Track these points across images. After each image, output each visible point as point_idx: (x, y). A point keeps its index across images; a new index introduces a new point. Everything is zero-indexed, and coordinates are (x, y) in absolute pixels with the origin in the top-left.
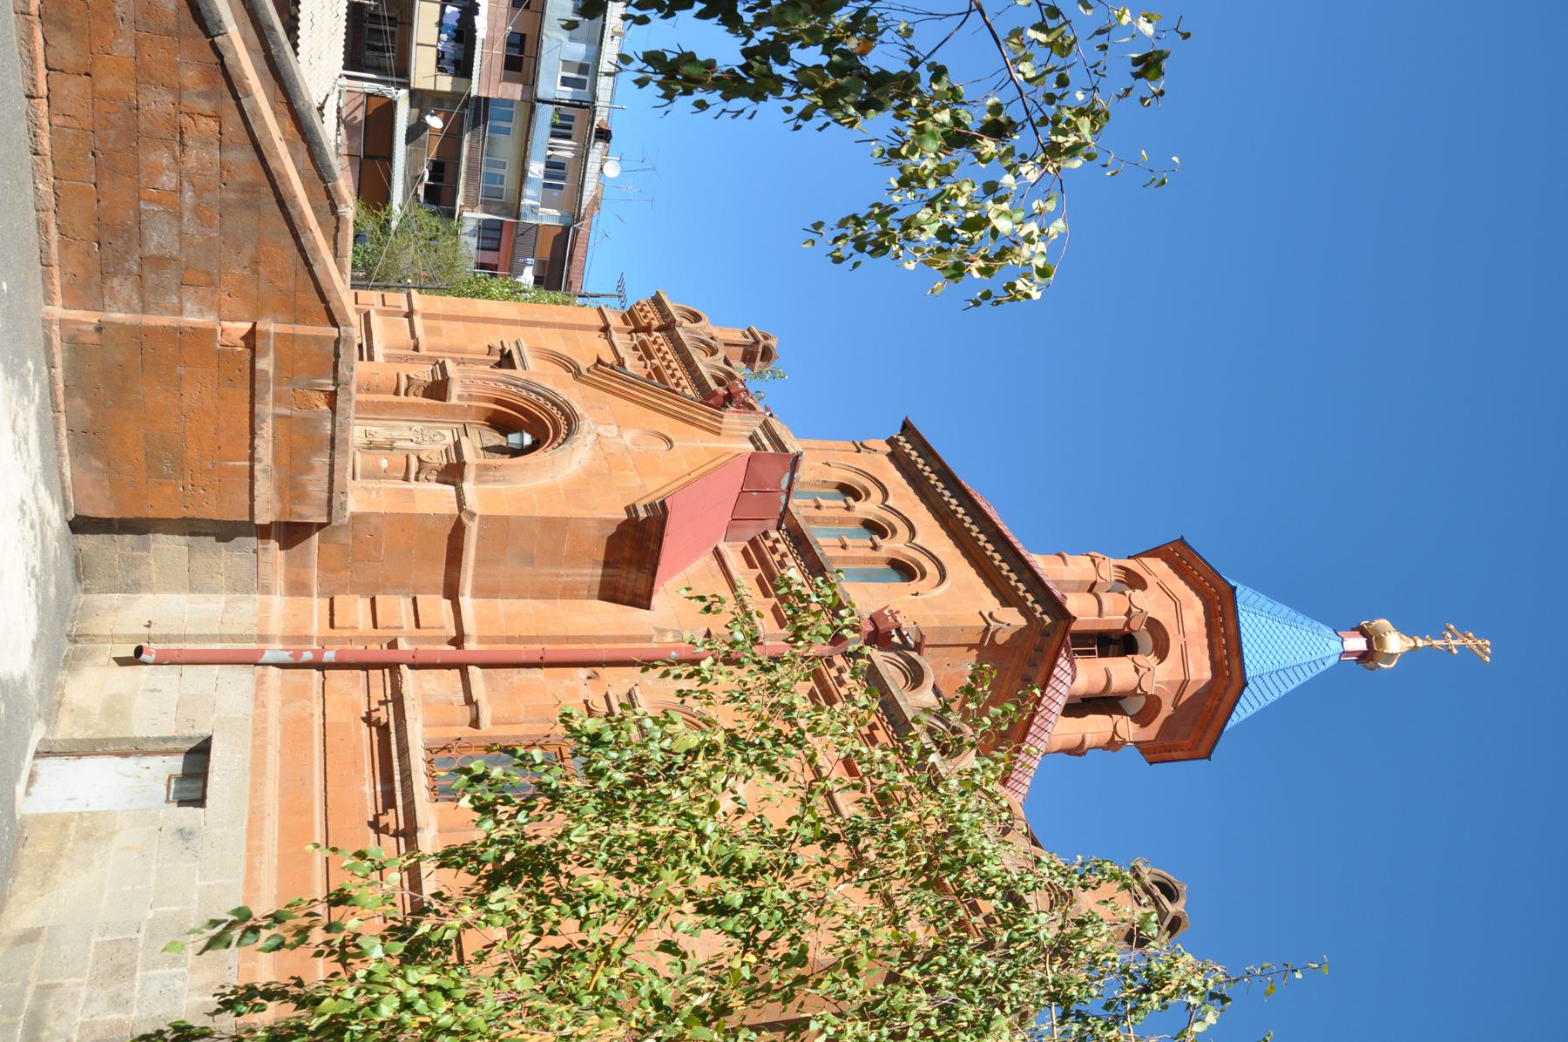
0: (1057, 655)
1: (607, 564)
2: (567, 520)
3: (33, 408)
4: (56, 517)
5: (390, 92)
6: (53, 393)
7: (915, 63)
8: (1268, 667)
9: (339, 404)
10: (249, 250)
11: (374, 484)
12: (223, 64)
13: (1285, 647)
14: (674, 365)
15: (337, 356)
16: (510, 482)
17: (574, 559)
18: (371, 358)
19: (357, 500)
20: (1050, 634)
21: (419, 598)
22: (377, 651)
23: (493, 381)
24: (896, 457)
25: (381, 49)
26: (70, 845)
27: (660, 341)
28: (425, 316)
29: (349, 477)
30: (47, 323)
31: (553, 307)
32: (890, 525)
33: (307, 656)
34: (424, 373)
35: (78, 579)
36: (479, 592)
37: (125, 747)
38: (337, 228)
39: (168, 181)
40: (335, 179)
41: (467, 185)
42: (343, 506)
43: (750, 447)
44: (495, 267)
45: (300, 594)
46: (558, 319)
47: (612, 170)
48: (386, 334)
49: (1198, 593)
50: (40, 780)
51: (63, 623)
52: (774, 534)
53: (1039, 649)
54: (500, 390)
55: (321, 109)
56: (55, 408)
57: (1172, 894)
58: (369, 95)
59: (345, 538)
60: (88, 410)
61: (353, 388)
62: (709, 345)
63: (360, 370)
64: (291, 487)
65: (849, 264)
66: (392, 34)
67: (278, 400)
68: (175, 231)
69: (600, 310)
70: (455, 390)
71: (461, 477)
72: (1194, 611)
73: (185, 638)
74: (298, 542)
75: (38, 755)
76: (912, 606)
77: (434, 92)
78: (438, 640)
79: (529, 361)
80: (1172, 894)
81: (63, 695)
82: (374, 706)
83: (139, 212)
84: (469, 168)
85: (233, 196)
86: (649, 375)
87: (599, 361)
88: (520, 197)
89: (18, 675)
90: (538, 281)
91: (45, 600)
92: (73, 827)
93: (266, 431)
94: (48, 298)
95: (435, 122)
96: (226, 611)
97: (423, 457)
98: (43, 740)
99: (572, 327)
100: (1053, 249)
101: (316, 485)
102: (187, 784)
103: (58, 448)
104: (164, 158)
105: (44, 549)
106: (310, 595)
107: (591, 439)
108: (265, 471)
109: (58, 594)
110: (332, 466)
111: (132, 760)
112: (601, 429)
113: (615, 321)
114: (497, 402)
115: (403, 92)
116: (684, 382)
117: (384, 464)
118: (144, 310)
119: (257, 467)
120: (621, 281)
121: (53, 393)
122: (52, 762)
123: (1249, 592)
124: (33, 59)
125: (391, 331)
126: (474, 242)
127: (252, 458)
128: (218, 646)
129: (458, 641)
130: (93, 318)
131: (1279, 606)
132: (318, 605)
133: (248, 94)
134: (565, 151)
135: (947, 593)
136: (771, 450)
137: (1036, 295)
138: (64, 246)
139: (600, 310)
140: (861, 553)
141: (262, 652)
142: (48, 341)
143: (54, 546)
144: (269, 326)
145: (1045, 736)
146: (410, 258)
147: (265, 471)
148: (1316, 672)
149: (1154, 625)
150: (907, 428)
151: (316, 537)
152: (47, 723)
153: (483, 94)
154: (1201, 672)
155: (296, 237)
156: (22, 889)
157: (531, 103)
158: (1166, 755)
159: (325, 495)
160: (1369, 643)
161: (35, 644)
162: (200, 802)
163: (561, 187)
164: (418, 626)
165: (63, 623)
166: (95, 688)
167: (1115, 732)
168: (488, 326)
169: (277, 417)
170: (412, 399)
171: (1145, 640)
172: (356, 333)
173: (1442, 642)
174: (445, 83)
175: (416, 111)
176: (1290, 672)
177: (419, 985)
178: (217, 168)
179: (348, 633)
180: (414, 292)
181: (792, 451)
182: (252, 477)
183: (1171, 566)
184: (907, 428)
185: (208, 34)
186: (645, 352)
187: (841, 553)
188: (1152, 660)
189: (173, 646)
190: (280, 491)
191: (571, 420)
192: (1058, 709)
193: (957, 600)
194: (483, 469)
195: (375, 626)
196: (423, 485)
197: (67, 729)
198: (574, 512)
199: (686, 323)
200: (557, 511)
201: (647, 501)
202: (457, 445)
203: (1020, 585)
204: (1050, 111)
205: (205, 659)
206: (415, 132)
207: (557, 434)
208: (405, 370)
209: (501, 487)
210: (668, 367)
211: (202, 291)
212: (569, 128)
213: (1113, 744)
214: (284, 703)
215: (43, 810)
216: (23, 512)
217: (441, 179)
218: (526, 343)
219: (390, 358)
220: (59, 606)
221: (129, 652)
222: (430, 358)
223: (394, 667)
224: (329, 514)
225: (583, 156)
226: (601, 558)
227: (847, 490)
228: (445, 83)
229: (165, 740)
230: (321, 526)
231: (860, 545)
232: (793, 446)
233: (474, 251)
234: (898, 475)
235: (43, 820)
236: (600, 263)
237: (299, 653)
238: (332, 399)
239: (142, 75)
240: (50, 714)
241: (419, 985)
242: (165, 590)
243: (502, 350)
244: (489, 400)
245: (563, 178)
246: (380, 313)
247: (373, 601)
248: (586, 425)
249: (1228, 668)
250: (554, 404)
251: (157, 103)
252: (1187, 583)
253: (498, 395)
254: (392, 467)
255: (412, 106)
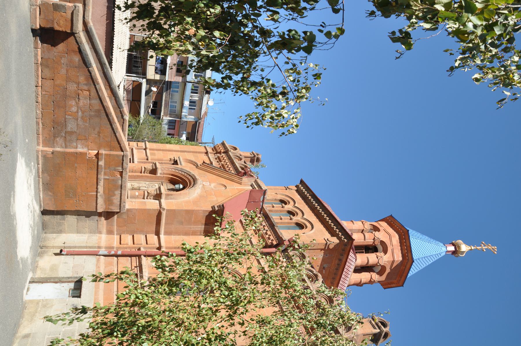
0: (349, 251)
1: (206, 224)
2: (193, 211)
3: (33, 176)
4: (38, 210)
5: (141, 80)
6: (38, 172)
7: (263, 78)
8: (421, 256)
9: (124, 175)
10: (97, 129)
11: (134, 200)
12: (91, 76)
13: (426, 250)
14: (228, 164)
15: (123, 160)
16: (176, 199)
17: (196, 223)
18: (133, 162)
19: (128, 205)
20: (347, 245)
21: (148, 235)
22: (134, 251)
23: (171, 169)
24: (298, 191)
25: (137, 67)
26: (39, 309)
27: (224, 156)
28: (150, 149)
29: (126, 197)
30: (38, 151)
31: (191, 146)
32: (296, 212)
33: (113, 253)
34: (149, 167)
35: (43, 229)
36: (166, 233)
37: (56, 280)
38: (123, 123)
39: (74, 109)
40: (123, 108)
41: (164, 109)
42: (124, 206)
43: (251, 188)
44: (173, 135)
45: (111, 234)
46: (192, 150)
47: (211, 103)
48: (138, 155)
49: (397, 232)
50: (31, 290)
51: (38, 242)
52: (259, 215)
53: (343, 250)
54: (173, 171)
55: (119, 86)
56: (39, 177)
57: (385, 325)
58: (134, 81)
59: (125, 216)
60: (48, 177)
61: (128, 170)
62: (239, 157)
63: (130, 166)
64: (108, 200)
65: (250, 128)
66: (141, 62)
67: (105, 174)
68: (76, 124)
69: (205, 147)
70: (159, 171)
71: (161, 198)
72: (396, 238)
73: (75, 247)
74: (110, 218)
75: (30, 282)
76: (305, 237)
77: (154, 80)
78: (153, 248)
79: (183, 163)
80: (385, 325)
81: (38, 264)
82: (133, 268)
83: (65, 118)
84: (165, 103)
85: (93, 113)
86: (220, 167)
87: (204, 162)
88: (181, 112)
89: (26, 257)
90: (187, 139)
91: (34, 235)
92: (40, 304)
93: (101, 183)
94: (38, 144)
95: (154, 89)
96: (88, 239)
97: (149, 192)
98: (32, 278)
99: (196, 152)
100: (298, 120)
101: (116, 200)
102: (75, 291)
103: (39, 189)
104: (74, 103)
105: (34, 219)
106: (114, 234)
107: (201, 186)
108: (101, 196)
109: (37, 233)
110: (121, 194)
111: (58, 284)
112: (204, 183)
113: (210, 150)
114: (172, 175)
115: (144, 80)
116: (231, 169)
117: (137, 194)
118: (66, 147)
119: (98, 194)
120: (213, 138)
121: (38, 172)
122: (34, 284)
123: (414, 232)
124: (38, 76)
125: (139, 154)
126: (166, 127)
127: (97, 192)
128: (85, 250)
129: (159, 248)
130: (51, 150)
131: (424, 236)
132: (116, 237)
133: (98, 84)
134: (196, 97)
135: (314, 233)
136: (257, 189)
137: (295, 132)
138: (43, 129)
139: (205, 147)
140: (287, 221)
141: (99, 251)
142: (38, 157)
143: (37, 218)
144: (103, 152)
145: (348, 279)
146: (146, 131)
147: (101, 196)
148: (438, 258)
149: (382, 243)
150: (302, 182)
151: (116, 216)
152: (33, 273)
153: (169, 80)
154: (398, 257)
155: (111, 125)
156: (25, 322)
157: (185, 83)
158: (389, 286)
159: (119, 203)
160: (455, 248)
161: (31, 248)
162: (79, 296)
163: (194, 109)
164: (147, 244)
165: (38, 242)
166: (48, 262)
167: (371, 278)
168: (170, 152)
169: (105, 179)
170: (146, 174)
171: (380, 248)
172: (129, 153)
173: (480, 248)
174: (158, 77)
175: (148, 86)
176: (429, 258)
177: (140, 293)
178: (88, 105)
179: (125, 246)
180: (147, 142)
181: (264, 189)
182: (97, 197)
183: (388, 224)
184: (302, 182)
185: (87, 67)
186: (219, 160)
187: (280, 221)
188: (382, 254)
189: (71, 250)
190: (105, 202)
191: (195, 180)
192: (352, 270)
193: (318, 235)
194: (167, 195)
195: (134, 244)
196: (149, 200)
197: (39, 274)
198: (195, 208)
199: (232, 151)
200: (190, 208)
201: (218, 205)
202: (160, 188)
203: (337, 230)
204: (296, 88)
205: (81, 253)
206: (148, 92)
207: (190, 184)
208: (143, 165)
209: (173, 201)
210: (226, 164)
211: (83, 141)
212: (197, 90)
213: (371, 282)
214: (105, 267)
215: (31, 298)
216: (29, 208)
217: (156, 107)
218: (182, 157)
219: (139, 162)
220: (38, 237)
221: (58, 251)
222: (152, 162)
223: (139, 256)
224: (120, 209)
225: (201, 99)
226: (204, 222)
227: (283, 202)
228: (158, 77)
229: (69, 278)
230: (117, 213)
231: (286, 219)
232: (264, 187)
233: (167, 130)
234: (299, 197)
235: (31, 301)
236: (208, 133)
237: (110, 252)
238: (121, 173)
239: (68, 79)
240: (34, 270)
241: (140, 293)
242: (69, 233)
243: (174, 160)
244: (170, 174)
245: (195, 106)
246: (136, 149)
247: (133, 236)
248: (199, 181)
249: (407, 256)
250: (190, 175)
251: (72, 87)
252: (393, 229)
253: (172, 173)
254: (139, 195)
255: (147, 84)
